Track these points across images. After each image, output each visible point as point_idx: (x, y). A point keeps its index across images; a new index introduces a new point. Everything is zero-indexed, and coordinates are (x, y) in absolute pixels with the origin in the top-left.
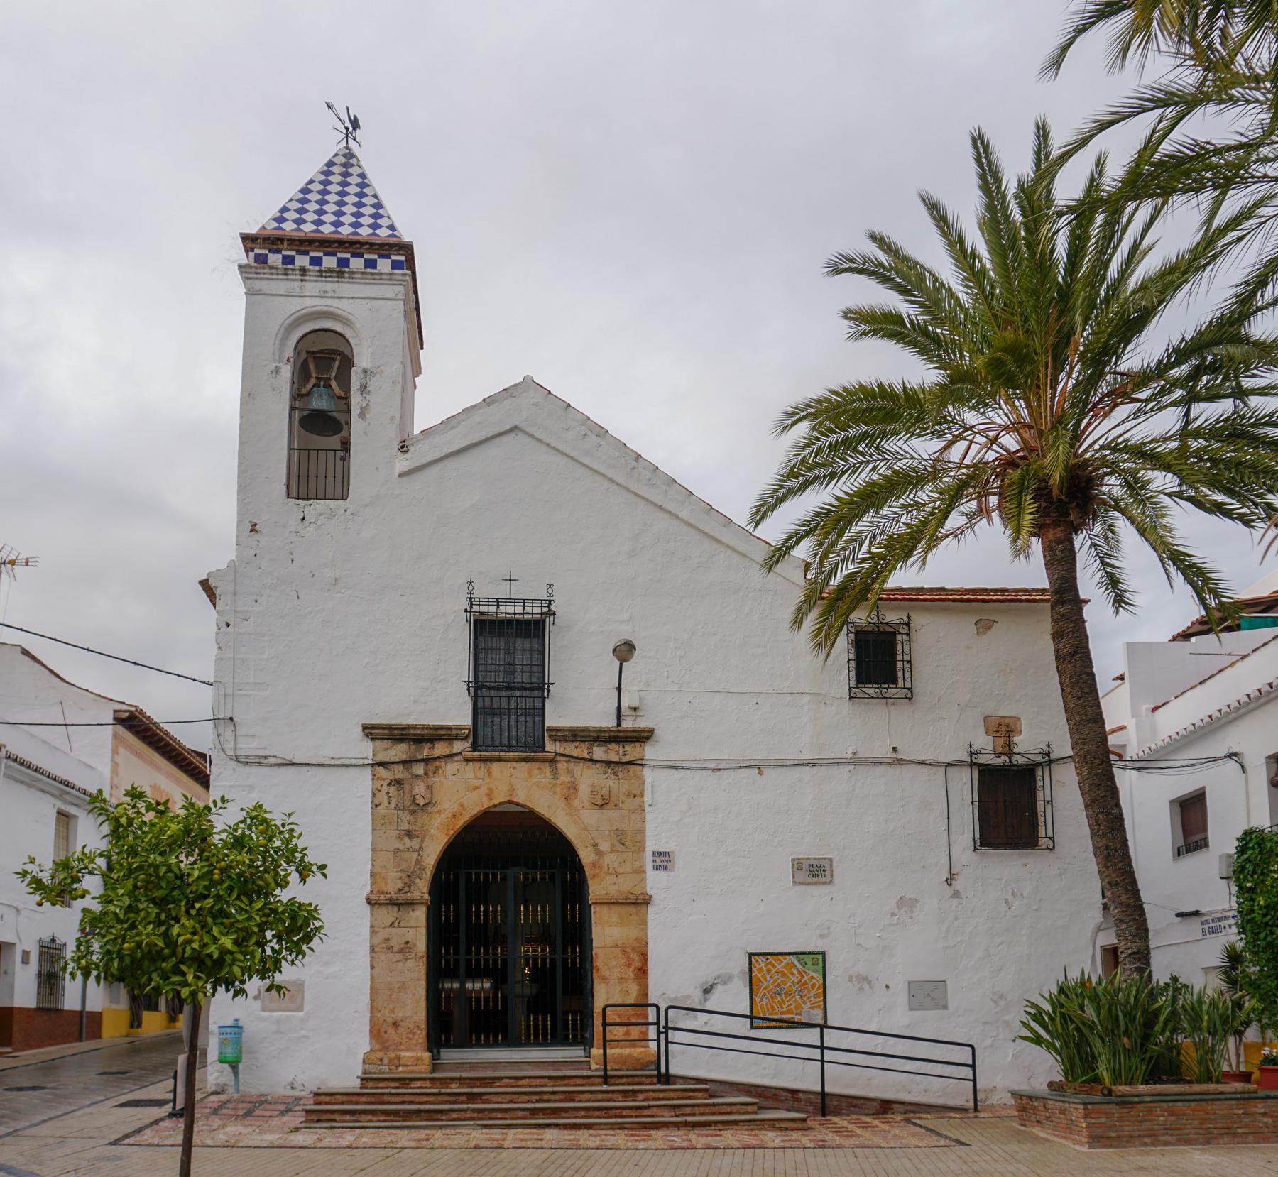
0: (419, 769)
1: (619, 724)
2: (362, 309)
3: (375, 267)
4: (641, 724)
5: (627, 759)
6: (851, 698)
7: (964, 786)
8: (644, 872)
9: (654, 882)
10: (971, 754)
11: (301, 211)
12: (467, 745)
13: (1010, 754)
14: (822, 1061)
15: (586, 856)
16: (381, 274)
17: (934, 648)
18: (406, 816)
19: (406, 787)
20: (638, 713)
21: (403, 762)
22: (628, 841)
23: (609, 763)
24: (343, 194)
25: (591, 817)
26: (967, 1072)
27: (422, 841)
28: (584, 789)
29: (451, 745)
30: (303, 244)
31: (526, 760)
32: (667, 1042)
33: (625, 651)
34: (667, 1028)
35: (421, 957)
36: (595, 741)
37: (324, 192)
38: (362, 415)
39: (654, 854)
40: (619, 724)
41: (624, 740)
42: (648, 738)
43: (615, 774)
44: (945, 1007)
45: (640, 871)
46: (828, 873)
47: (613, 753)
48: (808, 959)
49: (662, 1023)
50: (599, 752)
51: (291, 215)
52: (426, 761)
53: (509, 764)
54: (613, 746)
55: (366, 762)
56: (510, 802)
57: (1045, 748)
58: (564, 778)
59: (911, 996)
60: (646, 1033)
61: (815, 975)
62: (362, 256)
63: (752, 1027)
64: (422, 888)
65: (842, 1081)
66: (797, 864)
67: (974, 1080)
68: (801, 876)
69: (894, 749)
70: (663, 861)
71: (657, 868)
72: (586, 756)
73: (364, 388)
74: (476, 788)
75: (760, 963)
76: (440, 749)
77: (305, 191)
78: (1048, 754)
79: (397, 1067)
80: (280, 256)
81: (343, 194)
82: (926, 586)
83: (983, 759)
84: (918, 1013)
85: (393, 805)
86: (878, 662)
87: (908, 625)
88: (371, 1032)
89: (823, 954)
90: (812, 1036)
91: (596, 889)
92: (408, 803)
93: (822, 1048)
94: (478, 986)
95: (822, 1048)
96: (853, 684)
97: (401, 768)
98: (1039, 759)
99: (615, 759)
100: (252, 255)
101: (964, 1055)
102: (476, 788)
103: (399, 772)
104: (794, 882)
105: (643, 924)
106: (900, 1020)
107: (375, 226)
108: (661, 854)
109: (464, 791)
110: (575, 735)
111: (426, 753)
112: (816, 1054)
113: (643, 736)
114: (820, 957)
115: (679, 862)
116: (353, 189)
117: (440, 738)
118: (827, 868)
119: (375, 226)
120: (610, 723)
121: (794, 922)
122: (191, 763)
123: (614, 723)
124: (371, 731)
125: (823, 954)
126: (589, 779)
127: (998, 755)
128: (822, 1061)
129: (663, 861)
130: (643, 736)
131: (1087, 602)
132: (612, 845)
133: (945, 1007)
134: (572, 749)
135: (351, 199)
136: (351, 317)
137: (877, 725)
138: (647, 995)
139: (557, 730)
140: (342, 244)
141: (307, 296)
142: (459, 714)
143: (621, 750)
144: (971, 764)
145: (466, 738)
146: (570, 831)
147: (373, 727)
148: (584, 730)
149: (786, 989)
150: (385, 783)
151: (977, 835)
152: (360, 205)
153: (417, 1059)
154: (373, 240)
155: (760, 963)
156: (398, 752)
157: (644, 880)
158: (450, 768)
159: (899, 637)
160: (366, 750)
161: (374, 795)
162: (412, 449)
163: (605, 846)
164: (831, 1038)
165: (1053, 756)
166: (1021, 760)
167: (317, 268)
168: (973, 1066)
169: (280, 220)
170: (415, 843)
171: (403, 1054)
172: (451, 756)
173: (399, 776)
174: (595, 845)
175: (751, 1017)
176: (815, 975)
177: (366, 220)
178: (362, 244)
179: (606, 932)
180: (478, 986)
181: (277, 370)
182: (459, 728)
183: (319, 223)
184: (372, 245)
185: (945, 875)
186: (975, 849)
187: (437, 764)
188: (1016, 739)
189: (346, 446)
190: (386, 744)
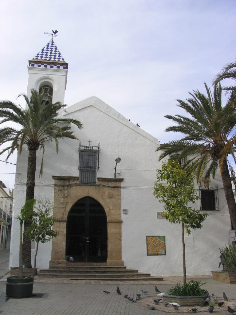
2: (55, 77)
3: (53, 68)
4: (120, 177)
9: (123, 217)
11: (42, 55)
25: (108, 200)
33: (118, 160)
39: (123, 210)
40: (115, 177)
45: (120, 215)
61: (163, 242)
64: (66, 217)
71: (124, 214)
72: (107, 185)
76: (71, 182)
77: (43, 50)
78: (217, 187)
80: (37, 65)
91: (108, 219)
103: (61, 188)
105: (120, 228)
107: (59, 59)
108: (125, 210)
109: (79, 192)
113: (121, 180)
115: (129, 212)
116: (54, 50)
120: (113, 177)
124: (54, 177)
126: (107, 191)
129: (126, 212)
130: (121, 180)
142: (75, 172)
146: (103, 204)
150: (57, 190)
156: (59, 183)
157: (121, 217)
163: (111, 208)
169: (37, 57)
176: (163, 242)
179: (111, 230)
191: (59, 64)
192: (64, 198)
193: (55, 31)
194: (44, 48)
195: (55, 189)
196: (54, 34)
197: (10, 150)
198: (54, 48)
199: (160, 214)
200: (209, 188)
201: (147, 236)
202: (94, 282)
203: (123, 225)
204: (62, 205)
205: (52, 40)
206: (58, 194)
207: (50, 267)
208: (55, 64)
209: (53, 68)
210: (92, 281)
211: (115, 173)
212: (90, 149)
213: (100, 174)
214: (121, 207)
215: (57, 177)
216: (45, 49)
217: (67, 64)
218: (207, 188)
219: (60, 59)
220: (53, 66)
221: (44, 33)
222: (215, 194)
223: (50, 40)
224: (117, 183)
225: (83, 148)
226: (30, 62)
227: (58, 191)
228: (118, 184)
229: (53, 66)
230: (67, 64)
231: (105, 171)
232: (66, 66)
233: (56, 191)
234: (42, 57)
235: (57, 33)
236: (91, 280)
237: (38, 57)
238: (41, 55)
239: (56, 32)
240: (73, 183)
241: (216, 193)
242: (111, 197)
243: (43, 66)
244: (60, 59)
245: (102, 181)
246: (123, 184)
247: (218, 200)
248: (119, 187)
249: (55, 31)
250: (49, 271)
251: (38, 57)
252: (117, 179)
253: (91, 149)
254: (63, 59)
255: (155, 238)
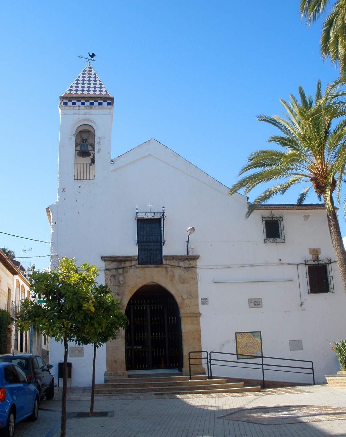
0: (121, 271)
1: (188, 254)
2: (96, 116)
3: (102, 105)
4: (195, 253)
5: (191, 266)
6: (265, 243)
7: (304, 271)
8: (198, 305)
9: (202, 309)
10: (305, 261)
11: (77, 87)
12: (137, 262)
13: (318, 260)
14: (263, 369)
15: (178, 300)
16: (104, 107)
17: (291, 224)
18: (116, 288)
19: (117, 277)
20: (194, 250)
21: (115, 269)
22: (193, 294)
23: (185, 267)
24: (89, 81)
26: (311, 371)
27: (122, 296)
28: (177, 276)
29: (131, 262)
30: (79, 99)
31: (157, 267)
32: (211, 364)
34: (210, 359)
35: (123, 337)
36: (180, 260)
37: (83, 80)
38: (99, 152)
39: (202, 299)
40: (188, 254)
41: (189, 260)
42: (198, 258)
43: (187, 271)
44: (302, 349)
45: (197, 305)
46: (261, 304)
47: (186, 264)
48: (255, 334)
49: (209, 358)
50: (181, 264)
51: (74, 89)
52: (123, 268)
53: (151, 269)
54: (186, 261)
55: (102, 269)
56: (152, 282)
57: (329, 258)
58: (170, 273)
59: (290, 346)
60: (201, 362)
61: (258, 339)
62: (97, 101)
63: (238, 359)
65: (269, 377)
66: (250, 301)
67: (313, 374)
68: (252, 304)
69: (280, 260)
70: (205, 301)
71: (203, 304)
72: (177, 265)
73: (99, 143)
74: (140, 277)
75: (259, 333)
76: (128, 264)
77: (78, 80)
78: (330, 260)
79: (117, 376)
80: (72, 102)
81: (89, 81)
82: (287, 204)
83: (309, 263)
84: (292, 351)
85: (112, 284)
86: (273, 230)
87: (282, 218)
88: (107, 364)
89: (260, 332)
90: (259, 361)
91: (182, 311)
92: (117, 283)
93: (262, 364)
94: (138, 347)
95: (262, 364)
96: (265, 238)
97: (114, 270)
98: (327, 262)
99: (187, 266)
100: (62, 103)
101: (309, 365)
102: (140, 277)
103: (114, 272)
104: (249, 307)
105: (199, 324)
106: (289, 354)
107: (101, 91)
108: (204, 299)
110: (173, 258)
111: (123, 266)
112: (261, 366)
113: (195, 258)
114: (259, 333)
115: (210, 301)
116: (92, 79)
117: (127, 260)
118: (260, 302)
119: (101, 91)
120: (184, 253)
121: (250, 321)
122: (8, 263)
123: (186, 253)
124: (103, 258)
125: (260, 332)
126: (178, 272)
127: (314, 261)
128: (263, 369)
129: (205, 301)
130: (195, 258)
131: (338, 215)
132: (187, 296)
133: (302, 349)
134: (175, 263)
135: (92, 82)
136: (94, 121)
137: (273, 250)
138: (201, 349)
139: (167, 256)
140: (91, 98)
141: (81, 115)
142: (133, 251)
143: (189, 263)
144: (306, 264)
145: (136, 260)
146: (173, 291)
147: (105, 257)
148: (177, 256)
149: (249, 346)
150: (109, 276)
151: (309, 289)
152: (95, 84)
153: (123, 373)
154: (100, 96)
155: (239, 336)
156: (113, 265)
157: (198, 308)
158: (131, 271)
159: (279, 222)
160: (102, 264)
161: (106, 281)
162: (115, 163)
163: (185, 297)
164: (266, 361)
165: (332, 261)
166: (321, 262)
167: (84, 106)
168: (313, 369)
170: (120, 297)
171: (118, 372)
172: (131, 266)
173: (114, 274)
174: (182, 296)
175: (237, 354)
176: (258, 339)
177: (98, 89)
178: (98, 98)
179: (186, 327)
180: (138, 347)
181: (71, 138)
182: (134, 257)
183: (83, 91)
184: (101, 98)
185: (300, 303)
186: (309, 293)
187: (127, 269)
188: (319, 256)
189: (93, 161)
190: (109, 262)
191: (101, 98)
192: (119, 286)
193: (91, 54)
194: (79, 77)
195: (105, 274)
196: (90, 58)
197: (285, 425)
198: (93, 76)
199: (253, 301)
200: (320, 262)
201: (236, 333)
202: (168, 397)
203: (202, 319)
204: (117, 296)
205: (89, 65)
206: (111, 281)
207: (106, 381)
208: (96, 99)
209: (102, 105)
210: (165, 395)
211: (188, 249)
212: (150, 216)
213: (167, 251)
214: (197, 295)
215: (107, 258)
216: (81, 79)
217: (112, 99)
218: (316, 262)
219: (102, 91)
220: (76, 102)
221: (79, 57)
222: (328, 270)
223: (87, 66)
224: (191, 262)
225: (142, 216)
226: (62, 98)
227: (111, 277)
228: (192, 263)
229: (76, 102)
230: (112, 99)
231: (172, 247)
232: (111, 101)
233: (107, 277)
234: (77, 90)
235: (94, 57)
236: (162, 394)
237: (72, 90)
238: (76, 87)
239: (93, 56)
240: (130, 265)
241: (329, 267)
242: (183, 281)
243: (89, 103)
244: (102, 91)
245: (170, 260)
246: (199, 263)
247: (332, 278)
248: (195, 267)
249: (91, 54)
250: (105, 385)
251: (72, 90)
252: (191, 256)
253: (153, 215)
254: (106, 91)
255: (247, 335)
